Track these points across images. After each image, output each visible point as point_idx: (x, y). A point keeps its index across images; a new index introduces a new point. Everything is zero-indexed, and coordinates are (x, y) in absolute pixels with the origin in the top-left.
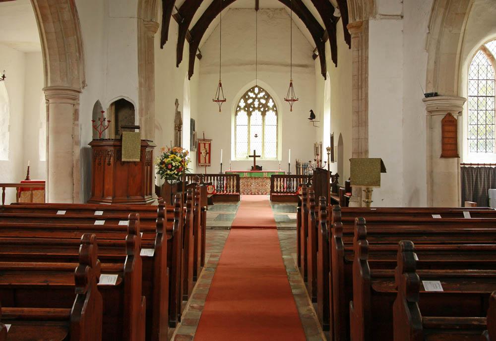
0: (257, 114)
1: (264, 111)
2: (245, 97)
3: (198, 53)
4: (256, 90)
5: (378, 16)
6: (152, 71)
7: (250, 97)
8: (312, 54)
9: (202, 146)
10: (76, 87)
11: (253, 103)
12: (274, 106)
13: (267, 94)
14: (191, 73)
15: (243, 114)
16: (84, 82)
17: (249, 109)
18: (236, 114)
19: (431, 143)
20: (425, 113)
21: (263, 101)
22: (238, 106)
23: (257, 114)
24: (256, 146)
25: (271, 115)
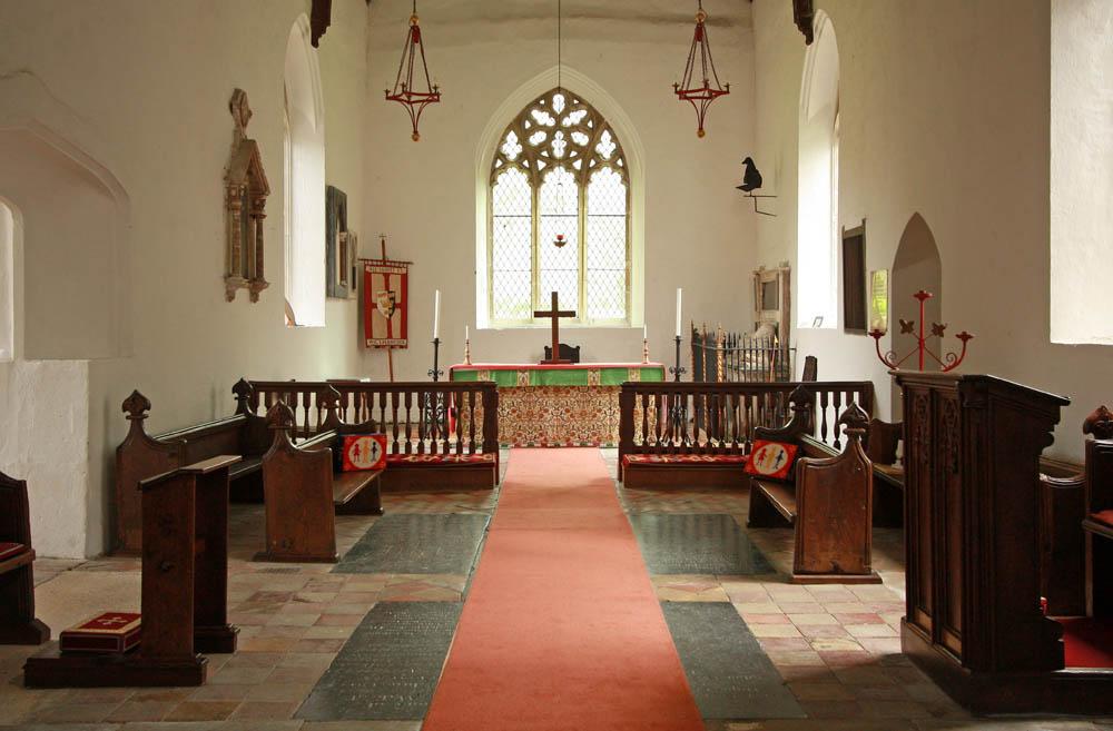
0: (559, 183)
1: (584, 165)
2: (520, 125)
4: (559, 102)
7: (536, 127)
9: (377, 282)
11: (547, 145)
12: (618, 153)
13: (593, 114)
15: (513, 182)
17: (534, 164)
18: (492, 181)
21: (581, 139)
22: (500, 155)
23: (559, 183)
24: (559, 277)
25: (606, 183)
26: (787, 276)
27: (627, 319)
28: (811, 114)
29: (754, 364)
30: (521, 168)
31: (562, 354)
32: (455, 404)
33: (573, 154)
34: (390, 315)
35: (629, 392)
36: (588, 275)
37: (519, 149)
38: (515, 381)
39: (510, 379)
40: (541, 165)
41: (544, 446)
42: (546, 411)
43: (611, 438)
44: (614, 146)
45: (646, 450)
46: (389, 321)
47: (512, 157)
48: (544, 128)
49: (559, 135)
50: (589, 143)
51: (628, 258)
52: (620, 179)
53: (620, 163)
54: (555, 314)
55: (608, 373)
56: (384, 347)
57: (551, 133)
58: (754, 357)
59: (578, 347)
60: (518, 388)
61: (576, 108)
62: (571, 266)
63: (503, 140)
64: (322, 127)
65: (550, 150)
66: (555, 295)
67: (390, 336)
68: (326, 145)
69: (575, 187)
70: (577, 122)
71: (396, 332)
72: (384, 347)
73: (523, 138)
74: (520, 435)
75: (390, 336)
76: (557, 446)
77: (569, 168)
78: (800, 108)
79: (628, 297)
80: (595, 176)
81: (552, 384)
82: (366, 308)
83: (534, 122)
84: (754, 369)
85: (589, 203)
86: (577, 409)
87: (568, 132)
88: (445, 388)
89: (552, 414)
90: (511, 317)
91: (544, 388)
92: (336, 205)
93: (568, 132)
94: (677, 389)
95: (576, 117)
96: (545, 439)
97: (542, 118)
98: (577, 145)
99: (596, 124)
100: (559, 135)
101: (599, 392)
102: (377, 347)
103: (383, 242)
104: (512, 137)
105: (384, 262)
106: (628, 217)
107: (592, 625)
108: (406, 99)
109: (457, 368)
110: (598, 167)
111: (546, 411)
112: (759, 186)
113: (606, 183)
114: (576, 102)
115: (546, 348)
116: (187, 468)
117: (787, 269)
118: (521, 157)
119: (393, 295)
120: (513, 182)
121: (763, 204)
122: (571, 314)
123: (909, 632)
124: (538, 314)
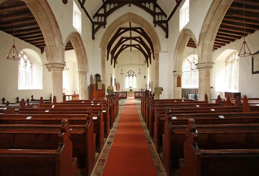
0: (131, 77)
1: (133, 76)
2: (128, 73)
3: (116, 62)
4: (131, 71)
5: (161, 52)
6: (105, 67)
7: (129, 73)
8: (145, 62)
9: (117, 85)
10: (86, 71)
11: (130, 74)
12: (136, 75)
13: (134, 72)
14: (114, 67)
15: (128, 77)
16: (88, 70)
17: (129, 76)
18: (126, 77)
19: (174, 83)
20: (173, 76)
21: (133, 74)
22: (126, 75)
23: (131, 77)
24: (131, 85)
25: (135, 77)
31: (131, 90)
35: (135, 92)
45: (136, 96)
54: (131, 87)
57: (130, 73)
69: (15, 45)
88: (123, 92)
89: (130, 94)
92: (115, 79)
94: (139, 92)
108: (152, 8)
116: (141, 32)
121: (146, 79)
123: (76, 31)
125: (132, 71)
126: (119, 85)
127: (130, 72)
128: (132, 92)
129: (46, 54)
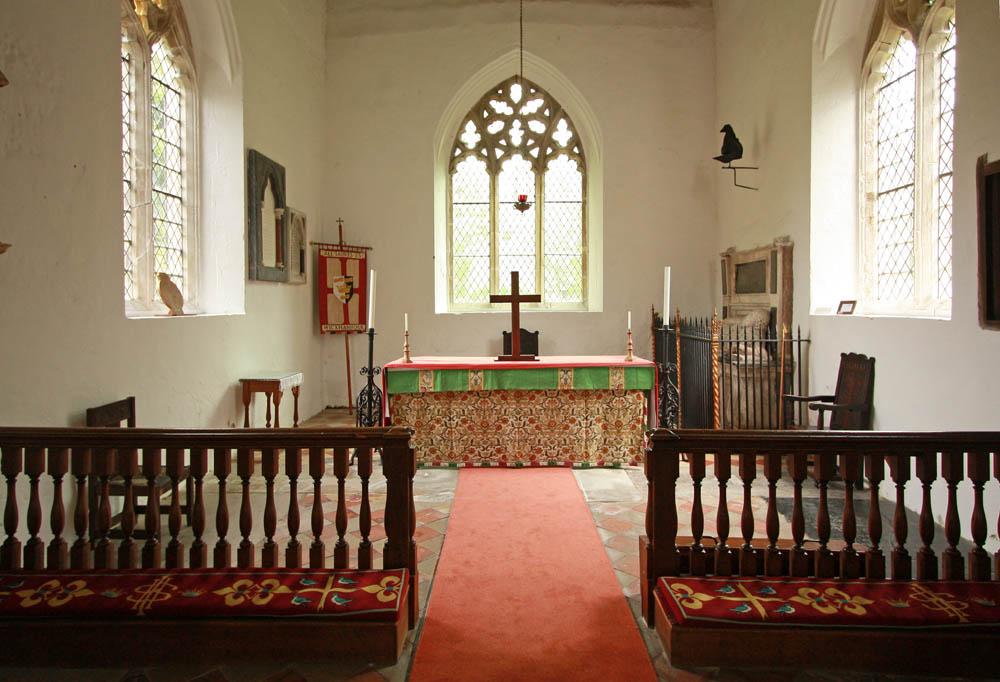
0: (517, 173)
2: (480, 113)
4: (516, 92)
9: (333, 267)
12: (575, 141)
15: (472, 169)
17: (492, 151)
18: (452, 169)
21: (537, 127)
22: (459, 144)
23: (517, 173)
24: (516, 254)
25: (563, 172)
26: (788, 253)
27: (584, 302)
28: (829, 52)
29: (750, 357)
30: (480, 156)
32: (390, 413)
33: (530, 142)
34: (347, 301)
36: (546, 262)
37: (478, 138)
38: (465, 382)
39: (460, 382)
40: (499, 153)
41: (503, 466)
42: (505, 421)
43: (587, 455)
44: (570, 134)
46: (346, 307)
47: (471, 145)
48: (501, 117)
49: (517, 124)
50: (546, 132)
51: (585, 242)
52: (576, 166)
53: (576, 150)
54: (515, 298)
55: (584, 373)
56: (339, 332)
57: (508, 121)
58: (750, 349)
59: (537, 333)
60: (470, 392)
61: (534, 97)
62: (528, 252)
63: (462, 129)
64: (239, 79)
65: (508, 138)
66: (515, 276)
67: (347, 322)
68: (244, 101)
69: (532, 175)
70: (534, 111)
71: (354, 317)
72: (339, 332)
73: (481, 128)
74: (472, 452)
75: (347, 322)
76: (519, 466)
77: (526, 156)
78: (814, 47)
79: (584, 282)
80: (551, 164)
81: (513, 387)
82: (321, 292)
83: (492, 111)
84: (750, 362)
85: (547, 189)
86: (544, 419)
87: (525, 120)
90: (471, 301)
91: (503, 393)
93: (525, 120)
95: (533, 106)
96: (504, 457)
97: (499, 107)
98: (535, 133)
99: (554, 111)
100: (517, 124)
101: (572, 398)
102: (333, 332)
103: (340, 227)
104: (471, 126)
105: (341, 246)
106: (584, 203)
107: (532, 578)
109: (392, 366)
110: (554, 155)
111: (505, 421)
112: (739, 156)
113: (563, 172)
114: (533, 91)
115: (504, 333)
117: (789, 244)
118: (480, 145)
119: (348, 280)
120: (472, 169)
122: (536, 299)
124: (495, 299)
125: (525, 98)
126: (353, 269)
127: (509, 111)
128: (527, 383)
129: (601, 465)
